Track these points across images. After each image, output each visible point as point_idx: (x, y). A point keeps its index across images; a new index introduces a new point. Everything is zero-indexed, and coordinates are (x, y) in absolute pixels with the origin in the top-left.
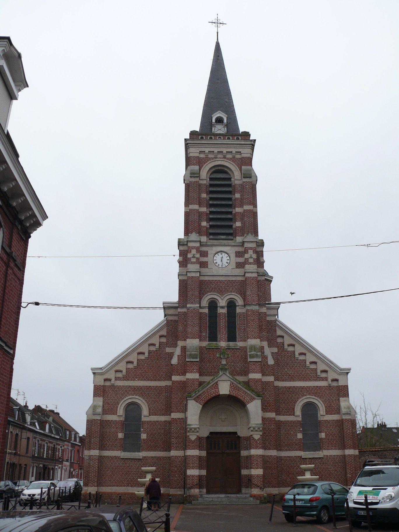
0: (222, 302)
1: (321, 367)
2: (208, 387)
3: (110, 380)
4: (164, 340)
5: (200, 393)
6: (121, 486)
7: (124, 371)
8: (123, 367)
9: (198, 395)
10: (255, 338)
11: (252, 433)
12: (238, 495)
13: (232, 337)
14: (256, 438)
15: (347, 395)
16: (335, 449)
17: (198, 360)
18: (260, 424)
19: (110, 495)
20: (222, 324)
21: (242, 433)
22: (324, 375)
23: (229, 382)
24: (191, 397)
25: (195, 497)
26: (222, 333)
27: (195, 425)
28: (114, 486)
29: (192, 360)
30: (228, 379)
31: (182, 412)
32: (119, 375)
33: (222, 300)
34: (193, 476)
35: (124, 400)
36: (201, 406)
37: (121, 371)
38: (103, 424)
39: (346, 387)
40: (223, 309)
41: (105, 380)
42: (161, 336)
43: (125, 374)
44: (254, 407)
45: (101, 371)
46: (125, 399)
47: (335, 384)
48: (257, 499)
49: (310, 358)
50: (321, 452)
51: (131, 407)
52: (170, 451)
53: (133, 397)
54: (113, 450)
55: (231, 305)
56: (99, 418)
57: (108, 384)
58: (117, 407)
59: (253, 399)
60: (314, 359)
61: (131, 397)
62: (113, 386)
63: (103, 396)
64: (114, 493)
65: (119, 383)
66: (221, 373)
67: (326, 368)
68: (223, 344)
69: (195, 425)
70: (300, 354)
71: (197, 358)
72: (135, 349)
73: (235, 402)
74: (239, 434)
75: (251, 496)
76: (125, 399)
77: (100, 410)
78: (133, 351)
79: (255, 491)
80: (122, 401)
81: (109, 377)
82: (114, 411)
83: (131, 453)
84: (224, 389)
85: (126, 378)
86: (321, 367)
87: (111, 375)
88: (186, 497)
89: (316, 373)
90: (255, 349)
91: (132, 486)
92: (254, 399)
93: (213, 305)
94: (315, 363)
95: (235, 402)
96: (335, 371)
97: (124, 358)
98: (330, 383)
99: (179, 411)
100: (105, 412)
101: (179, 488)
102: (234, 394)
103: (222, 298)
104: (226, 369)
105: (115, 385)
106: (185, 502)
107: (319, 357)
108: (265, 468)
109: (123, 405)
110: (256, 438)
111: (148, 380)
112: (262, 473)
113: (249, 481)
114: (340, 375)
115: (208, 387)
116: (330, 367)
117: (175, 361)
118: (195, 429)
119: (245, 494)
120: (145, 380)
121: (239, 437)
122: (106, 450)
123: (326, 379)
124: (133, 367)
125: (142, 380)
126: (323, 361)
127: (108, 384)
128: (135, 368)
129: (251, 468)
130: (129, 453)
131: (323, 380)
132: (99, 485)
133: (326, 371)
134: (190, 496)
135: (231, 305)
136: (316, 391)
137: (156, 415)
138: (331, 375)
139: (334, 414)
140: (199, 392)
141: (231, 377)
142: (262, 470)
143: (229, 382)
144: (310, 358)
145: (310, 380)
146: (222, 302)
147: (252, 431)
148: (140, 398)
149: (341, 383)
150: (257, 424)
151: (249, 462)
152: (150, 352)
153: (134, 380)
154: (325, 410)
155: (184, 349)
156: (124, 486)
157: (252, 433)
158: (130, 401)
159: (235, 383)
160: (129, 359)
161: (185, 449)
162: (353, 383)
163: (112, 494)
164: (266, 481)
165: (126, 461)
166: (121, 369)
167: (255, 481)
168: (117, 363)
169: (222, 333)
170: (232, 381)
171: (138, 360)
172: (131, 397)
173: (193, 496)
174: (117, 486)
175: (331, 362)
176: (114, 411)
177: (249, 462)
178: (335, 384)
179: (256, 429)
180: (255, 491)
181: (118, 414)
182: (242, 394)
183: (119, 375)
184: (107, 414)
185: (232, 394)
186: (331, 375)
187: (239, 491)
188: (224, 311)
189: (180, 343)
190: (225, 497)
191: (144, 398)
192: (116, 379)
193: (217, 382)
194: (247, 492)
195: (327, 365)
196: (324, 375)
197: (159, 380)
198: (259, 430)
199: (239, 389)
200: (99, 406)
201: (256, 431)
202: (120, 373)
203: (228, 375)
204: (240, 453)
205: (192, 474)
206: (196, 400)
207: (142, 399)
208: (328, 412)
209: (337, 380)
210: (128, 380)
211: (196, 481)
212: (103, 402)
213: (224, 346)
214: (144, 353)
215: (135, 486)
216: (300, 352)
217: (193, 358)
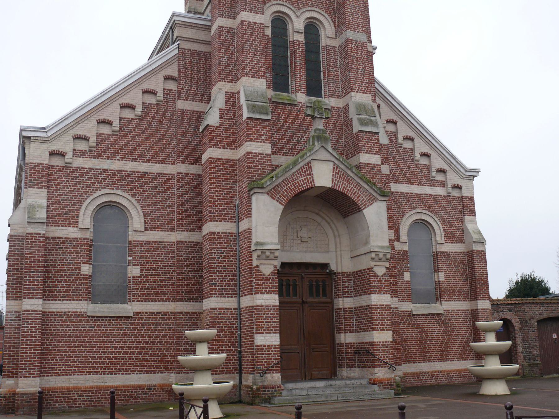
0: (297, 23)
1: (437, 163)
2: (294, 170)
3: (62, 155)
4: (172, 86)
5: (280, 180)
6: (89, 373)
7: (93, 139)
8: (90, 129)
9: (275, 184)
10: (362, 91)
11: (372, 264)
12: (333, 382)
13: (314, 89)
14: (380, 274)
15: (472, 213)
16: (459, 300)
17: (269, 117)
18: (387, 247)
19: (66, 393)
20: (298, 61)
21: (342, 263)
22: (440, 177)
23: (332, 164)
24: (262, 188)
25: (274, 390)
26: (298, 77)
27: (272, 243)
28: (74, 373)
29: (258, 116)
30: (328, 157)
31: (231, 220)
32: (82, 146)
33: (297, 17)
34: (269, 347)
35: (92, 197)
36: (282, 207)
37: (86, 139)
38: (51, 244)
39: (472, 199)
40: (299, 35)
41: (53, 154)
42: (167, 78)
43: (94, 144)
44: (375, 214)
45: (44, 135)
46: (95, 195)
47: (455, 193)
48: (385, 387)
49: (420, 147)
50: (438, 305)
51: (108, 211)
52: (201, 301)
53: (112, 191)
54: (70, 299)
55: (312, 29)
56: (41, 230)
57: (57, 162)
58: (78, 211)
59: (372, 200)
60: (426, 149)
61: (106, 191)
62: (68, 167)
63: (48, 188)
64: (75, 388)
65: (81, 163)
66: (317, 146)
67: (445, 167)
68: (301, 98)
69: (272, 243)
70: (407, 138)
71: (267, 114)
72: (116, 96)
73: (338, 205)
74: (333, 267)
75: (373, 382)
76: (95, 195)
77: (42, 215)
78: (111, 100)
79: (381, 373)
80: (89, 200)
81: (60, 148)
82: (72, 220)
83: (108, 305)
84: (323, 176)
85: (96, 153)
86: (437, 163)
87: (66, 145)
88: (258, 389)
89: (429, 172)
90: (365, 110)
91: (112, 373)
92: (375, 199)
93: (280, 23)
94: (428, 156)
95: (338, 205)
96: (457, 172)
97: (94, 111)
98: (450, 191)
99: (224, 219)
100: (51, 221)
101: (230, 372)
102: (341, 187)
103: (298, 14)
104: (326, 140)
105: (74, 165)
106: (257, 401)
107: (435, 146)
108: (396, 331)
109: (92, 208)
110: (380, 274)
111: (142, 160)
112: (391, 340)
113: (365, 355)
114: (464, 178)
115: (294, 170)
116: (450, 164)
117: (213, 119)
118: (272, 251)
119: (350, 379)
120: (135, 160)
121: (332, 273)
122: (56, 299)
123: (443, 184)
124: (110, 132)
125: (129, 159)
126: (440, 154)
127: (57, 162)
128: (115, 134)
129: (373, 329)
130: (103, 306)
131: (438, 186)
132: (43, 372)
133: (443, 171)
134: (264, 387)
135: (312, 29)
136: (428, 202)
137: (158, 229)
138: (452, 179)
139: (456, 242)
140: (277, 178)
141: (335, 154)
142: (390, 333)
143: (331, 164)
144: (420, 147)
145: (420, 184)
146: (297, 23)
147: (373, 259)
148: (125, 195)
149: (465, 193)
150: (382, 247)
151: (365, 318)
152: (145, 106)
153: (114, 158)
154: (443, 235)
155: (232, 99)
156: (97, 372)
157: (372, 264)
158: (105, 199)
159: (342, 167)
160: (104, 115)
161: (238, 295)
162: (481, 192)
163: (69, 390)
164: (400, 352)
165: (99, 322)
166: (85, 133)
167: (380, 354)
168: (78, 122)
169: (298, 77)
170: (336, 162)
171: (121, 119)
172: (106, 191)
173: (272, 387)
174: (81, 373)
175: (452, 156)
176: (72, 220)
177: (365, 318)
178: (455, 193)
179: (381, 255)
180: (381, 373)
181: (80, 226)
182: (353, 189)
183: (82, 146)
184: (56, 224)
185: (337, 188)
186: (452, 179)
187: (332, 375)
188: (301, 38)
189: (220, 92)
190: (326, 387)
191: (133, 196)
192: (77, 153)
193: (309, 164)
194: (352, 375)
195: (445, 159)
196: (440, 177)
197: (163, 162)
198: (384, 259)
199: (348, 179)
200: (41, 207)
201: (380, 259)
202: (84, 142)
203: (330, 149)
204: (332, 303)
205: (268, 343)
206: (273, 193)
207: (129, 197)
208: (449, 239)
209: (459, 187)
210: (100, 157)
211: (275, 356)
212: (48, 199)
213: (303, 101)
214: (132, 107)
215: (118, 372)
216: (405, 135)
217: (260, 113)
